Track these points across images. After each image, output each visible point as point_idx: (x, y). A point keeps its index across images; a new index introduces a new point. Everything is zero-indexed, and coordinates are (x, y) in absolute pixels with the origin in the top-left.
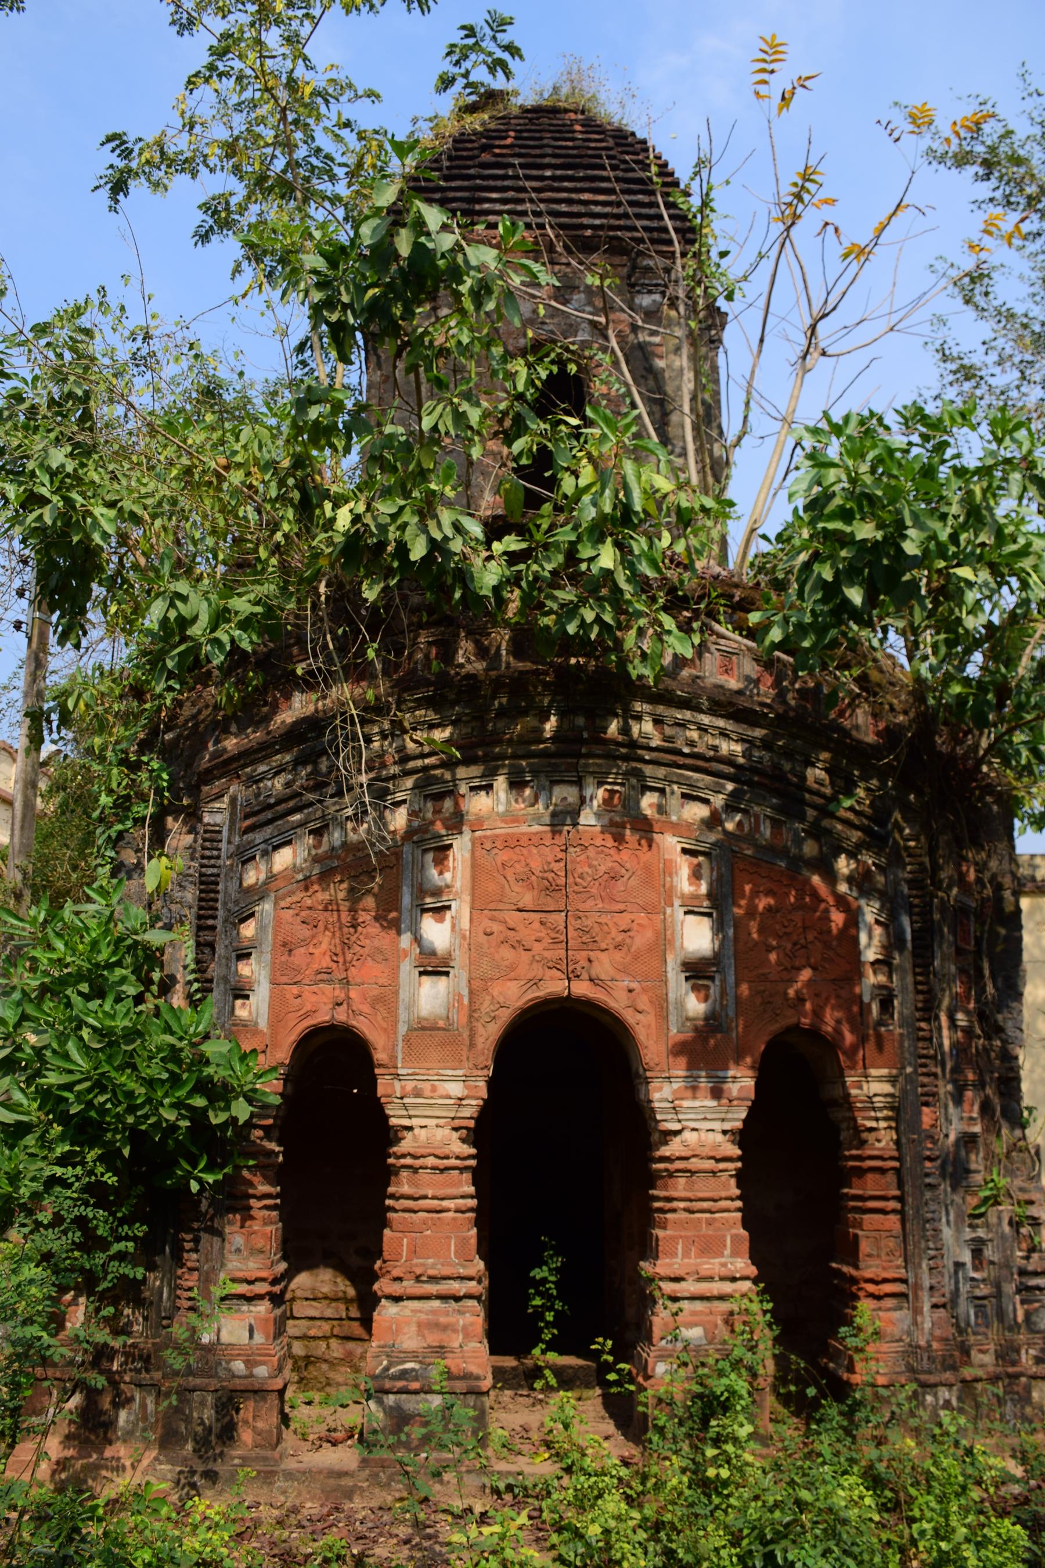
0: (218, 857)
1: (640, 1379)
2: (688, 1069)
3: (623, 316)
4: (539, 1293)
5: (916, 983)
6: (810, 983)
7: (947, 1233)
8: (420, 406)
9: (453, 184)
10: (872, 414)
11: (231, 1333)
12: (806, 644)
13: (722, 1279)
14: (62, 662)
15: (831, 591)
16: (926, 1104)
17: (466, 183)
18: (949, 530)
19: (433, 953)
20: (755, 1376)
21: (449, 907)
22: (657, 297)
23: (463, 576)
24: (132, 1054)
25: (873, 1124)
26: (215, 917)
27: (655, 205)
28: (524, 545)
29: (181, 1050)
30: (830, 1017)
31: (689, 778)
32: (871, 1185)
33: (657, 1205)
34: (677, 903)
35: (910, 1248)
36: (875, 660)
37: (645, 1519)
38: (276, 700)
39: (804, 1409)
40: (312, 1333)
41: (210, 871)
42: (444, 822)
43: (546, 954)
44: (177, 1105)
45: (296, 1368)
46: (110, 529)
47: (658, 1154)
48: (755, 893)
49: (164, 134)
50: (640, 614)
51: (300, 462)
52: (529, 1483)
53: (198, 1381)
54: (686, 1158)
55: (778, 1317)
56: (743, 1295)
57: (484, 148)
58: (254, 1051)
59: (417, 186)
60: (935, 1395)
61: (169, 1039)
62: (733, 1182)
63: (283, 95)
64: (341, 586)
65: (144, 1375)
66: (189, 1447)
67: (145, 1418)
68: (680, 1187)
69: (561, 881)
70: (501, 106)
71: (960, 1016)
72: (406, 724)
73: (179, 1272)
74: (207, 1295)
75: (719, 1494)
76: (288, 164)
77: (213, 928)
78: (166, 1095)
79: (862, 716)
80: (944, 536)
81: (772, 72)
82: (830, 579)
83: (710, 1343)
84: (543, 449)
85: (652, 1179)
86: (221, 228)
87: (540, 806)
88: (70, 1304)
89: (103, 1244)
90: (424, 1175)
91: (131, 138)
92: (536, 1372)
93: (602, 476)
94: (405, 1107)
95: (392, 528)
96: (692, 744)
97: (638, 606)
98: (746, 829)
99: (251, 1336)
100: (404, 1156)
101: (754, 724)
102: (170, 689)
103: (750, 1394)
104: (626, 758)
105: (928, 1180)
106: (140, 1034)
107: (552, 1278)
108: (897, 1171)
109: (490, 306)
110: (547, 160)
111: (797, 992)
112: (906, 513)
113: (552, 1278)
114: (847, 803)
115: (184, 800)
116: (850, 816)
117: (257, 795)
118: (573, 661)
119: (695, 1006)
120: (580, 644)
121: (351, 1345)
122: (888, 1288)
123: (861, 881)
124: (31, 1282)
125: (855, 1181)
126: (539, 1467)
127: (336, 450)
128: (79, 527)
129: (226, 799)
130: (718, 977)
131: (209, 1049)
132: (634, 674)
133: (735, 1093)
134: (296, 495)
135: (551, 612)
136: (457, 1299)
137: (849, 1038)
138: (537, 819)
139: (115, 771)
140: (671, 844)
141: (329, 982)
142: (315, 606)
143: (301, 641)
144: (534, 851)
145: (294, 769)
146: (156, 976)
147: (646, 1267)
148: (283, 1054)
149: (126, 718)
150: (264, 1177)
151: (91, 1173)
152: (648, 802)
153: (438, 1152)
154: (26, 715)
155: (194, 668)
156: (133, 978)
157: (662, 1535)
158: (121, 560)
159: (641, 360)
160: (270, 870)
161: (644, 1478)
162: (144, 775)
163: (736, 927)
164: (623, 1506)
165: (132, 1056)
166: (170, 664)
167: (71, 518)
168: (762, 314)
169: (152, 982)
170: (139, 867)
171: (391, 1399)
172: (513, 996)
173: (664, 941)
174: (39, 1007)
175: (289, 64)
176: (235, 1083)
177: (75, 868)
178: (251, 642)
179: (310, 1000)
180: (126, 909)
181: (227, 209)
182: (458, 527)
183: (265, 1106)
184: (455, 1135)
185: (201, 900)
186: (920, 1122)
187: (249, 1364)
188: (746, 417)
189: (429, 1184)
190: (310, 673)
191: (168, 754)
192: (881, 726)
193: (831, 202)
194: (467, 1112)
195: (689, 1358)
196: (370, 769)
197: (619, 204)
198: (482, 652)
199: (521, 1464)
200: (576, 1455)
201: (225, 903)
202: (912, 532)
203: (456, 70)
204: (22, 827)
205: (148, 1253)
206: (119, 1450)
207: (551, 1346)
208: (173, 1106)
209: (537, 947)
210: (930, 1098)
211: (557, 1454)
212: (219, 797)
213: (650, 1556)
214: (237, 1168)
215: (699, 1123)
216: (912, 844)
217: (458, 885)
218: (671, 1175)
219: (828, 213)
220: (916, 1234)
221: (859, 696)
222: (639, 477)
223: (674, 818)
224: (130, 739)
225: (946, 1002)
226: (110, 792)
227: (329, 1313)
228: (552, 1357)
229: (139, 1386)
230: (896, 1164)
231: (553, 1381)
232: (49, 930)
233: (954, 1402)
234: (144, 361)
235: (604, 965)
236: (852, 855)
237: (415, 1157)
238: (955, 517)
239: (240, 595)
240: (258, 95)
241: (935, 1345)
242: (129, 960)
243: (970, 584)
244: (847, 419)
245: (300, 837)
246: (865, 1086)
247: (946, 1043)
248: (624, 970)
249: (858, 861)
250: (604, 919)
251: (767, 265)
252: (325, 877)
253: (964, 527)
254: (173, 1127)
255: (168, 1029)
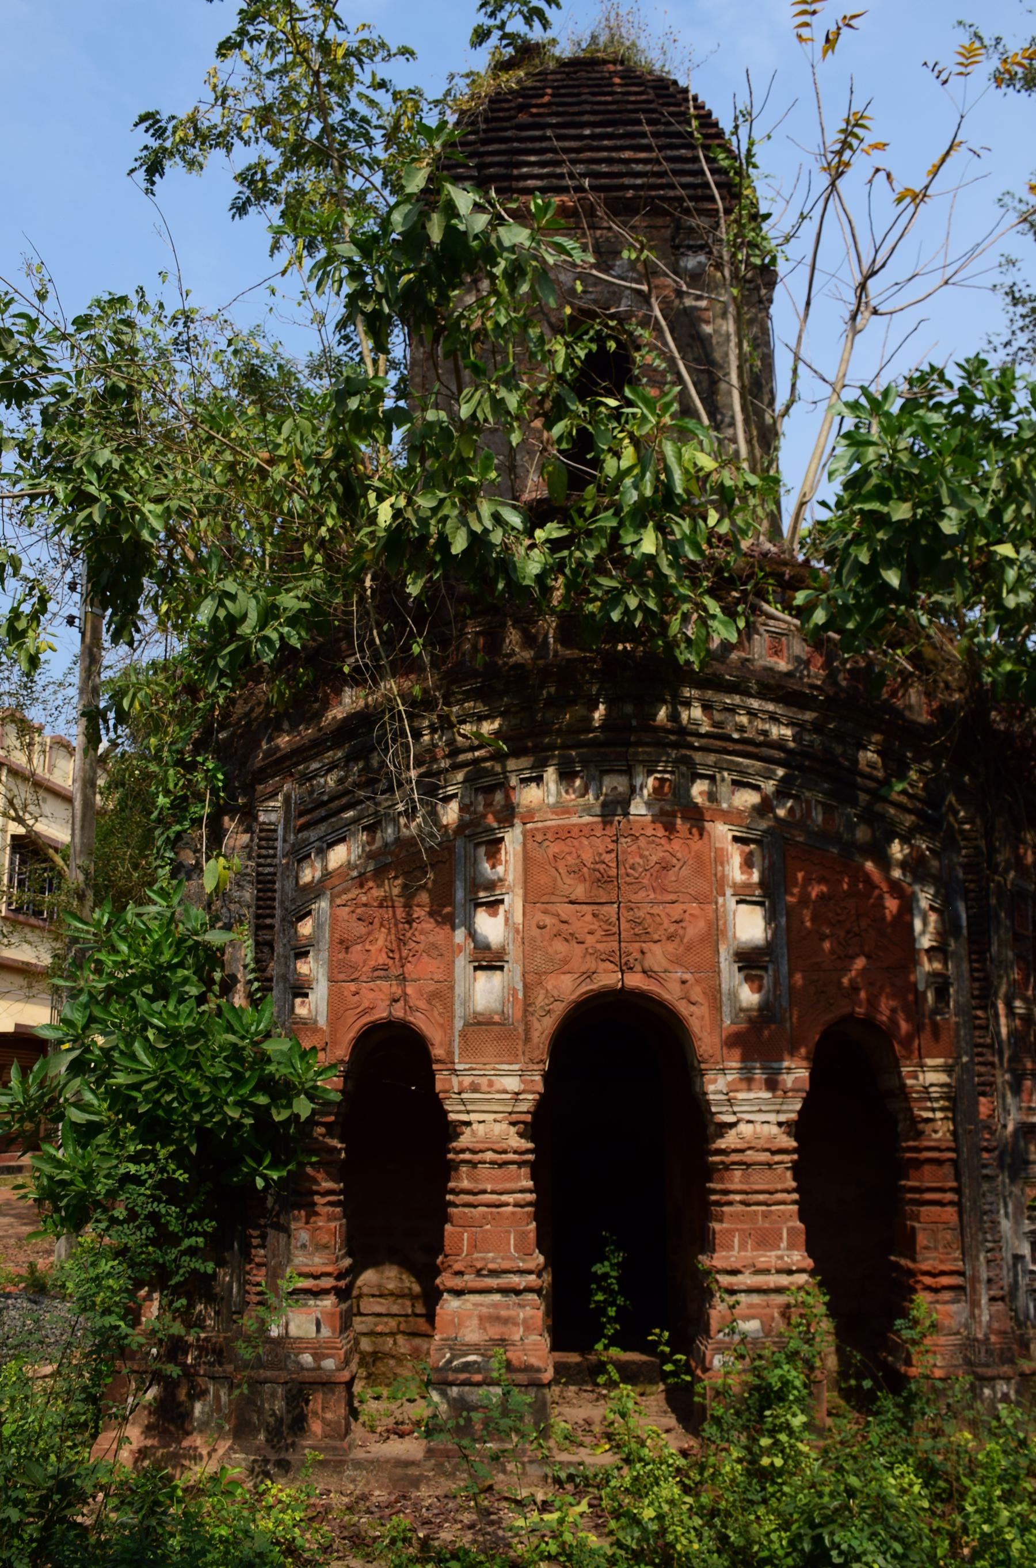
0: (274, 856)
1: (699, 1372)
2: (743, 1061)
3: (669, 281)
4: (600, 1289)
5: (972, 970)
6: (864, 971)
7: (1006, 1225)
8: (460, 391)
9: (490, 148)
10: (933, 368)
11: (299, 1327)
12: (850, 626)
13: (779, 1272)
14: (115, 658)
15: (869, 574)
16: (983, 1094)
17: (503, 147)
18: (988, 506)
19: (487, 947)
20: (812, 1368)
21: (502, 901)
22: (702, 258)
23: (506, 566)
24: (196, 1053)
25: (930, 1115)
26: (272, 916)
27: (696, 159)
28: (565, 532)
29: (244, 1048)
30: (885, 1006)
31: (739, 764)
32: (928, 1177)
33: (714, 1198)
34: (729, 892)
35: (968, 1240)
36: (928, 637)
37: (702, 1507)
38: (326, 695)
39: (862, 1402)
40: (379, 1329)
41: (267, 870)
42: (495, 814)
43: (599, 946)
44: (241, 1103)
45: (362, 1363)
46: (157, 525)
47: (715, 1146)
48: (808, 881)
49: (197, 109)
50: (686, 599)
51: (344, 451)
52: (590, 1473)
53: (269, 1373)
54: (741, 1151)
55: (833, 1310)
56: (800, 1288)
57: (522, 108)
58: (314, 1048)
59: (446, 169)
60: (993, 1389)
61: (231, 1038)
62: (789, 1174)
63: (316, 58)
64: (387, 578)
65: (217, 1368)
66: (262, 1437)
67: (219, 1409)
68: (736, 1179)
69: (613, 872)
70: (537, 61)
71: (1018, 1003)
72: (454, 719)
73: (248, 1267)
74: (275, 1289)
75: (774, 1483)
76: (323, 130)
77: (271, 927)
78: (230, 1094)
79: (914, 696)
80: (983, 512)
81: (814, 13)
82: (866, 562)
83: (767, 1336)
84: (582, 431)
85: (709, 1172)
86: (258, 199)
87: (590, 797)
88: (145, 1299)
89: (174, 1240)
90: (483, 1170)
91: (164, 116)
92: (600, 1368)
93: (642, 461)
94: (463, 1102)
95: (433, 522)
96: (741, 729)
97: (682, 590)
98: (798, 815)
99: (318, 1330)
100: (463, 1151)
101: (804, 707)
102: (222, 687)
103: (805, 1386)
104: (675, 745)
105: (985, 1172)
106: (203, 1034)
107: (614, 1274)
108: (954, 1162)
109: (525, 288)
110: (585, 118)
111: (851, 980)
112: (944, 491)
113: (614, 1274)
114: (899, 787)
115: (239, 800)
116: (904, 799)
117: (311, 793)
118: (620, 647)
119: (749, 997)
120: (624, 630)
121: (417, 1341)
122: (945, 1281)
123: (914, 866)
124: (109, 1275)
125: (912, 1173)
126: (599, 1458)
127: (376, 440)
128: (128, 525)
129: (280, 797)
130: (771, 967)
131: (270, 1047)
132: (681, 659)
133: (790, 1085)
134: (340, 488)
135: (596, 599)
136: (518, 1292)
137: (904, 1026)
138: (588, 810)
139: (171, 772)
140: (722, 832)
141: (386, 978)
142: (362, 599)
143: (348, 635)
144: (586, 842)
145: (346, 765)
146: (217, 976)
147: (704, 1261)
148: (342, 1051)
149: (181, 718)
150: (328, 1173)
151: (163, 1170)
152: (698, 790)
153: (496, 1147)
154: (83, 715)
155: (245, 667)
156: (195, 978)
157: (717, 1521)
158: (170, 554)
159: (687, 327)
160: (325, 868)
161: (702, 1468)
162: (199, 776)
163: (788, 915)
164: (677, 1490)
165: (195, 1056)
166: (221, 663)
167: (120, 516)
168: (808, 270)
169: (214, 982)
170: (198, 868)
171: (454, 1391)
172: (567, 989)
173: (716, 930)
174: (105, 1009)
175: (320, 26)
176: (296, 1080)
177: (136, 866)
178: (300, 638)
179: (367, 997)
180: (186, 910)
181: (264, 179)
182: (497, 518)
183: (327, 1103)
184: (513, 1130)
185: (258, 899)
186: (978, 1112)
187: (318, 1357)
188: (794, 385)
189: (488, 1179)
190: (356, 669)
191: (223, 754)
192: (935, 705)
193: (881, 146)
194: (524, 1107)
195: (747, 1349)
196: (418, 764)
197: (657, 162)
198: (529, 640)
199: (583, 1455)
200: (634, 1446)
201: (282, 902)
202: (951, 512)
203: (491, 22)
204: (83, 827)
205: (217, 1248)
206: (197, 1441)
207: (613, 1341)
208: (237, 1104)
209: (590, 940)
210: (987, 1088)
211: (618, 1446)
212: (273, 796)
213: (705, 1540)
214: (301, 1165)
215: (754, 1116)
216: (967, 827)
217: (510, 878)
218: (727, 1167)
219: (878, 158)
220: (974, 1228)
221: (911, 674)
222: (679, 456)
223: (725, 806)
224: (185, 740)
225: (1003, 989)
226: (167, 793)
227: (395, 1309)
228: (615, 1352)
229: (213, 1378)
230: (953, 1155)
231: (616, 1376)
232: (113, 933)
233: (1013, 1395)
234: (185, 345)
235: (657, 956)
236: (905, 840)
237: (474, 1152)
238: (996, 493)
239: (288, 591)
240: (290, 58)
241: (993, 1338)
242: (190, 960)
243: (1010, 562)
244: (886, 393)
245: (354, 834)
246: (921, 1076)
247: (1004, 1031)
248: (677, 961)
249: (912, 846)
250: (656, 910)
251: (809, 228)
252: (379, 874)
253: (1007, 500)
254: (238, 1125)
255: (230, 1029)
